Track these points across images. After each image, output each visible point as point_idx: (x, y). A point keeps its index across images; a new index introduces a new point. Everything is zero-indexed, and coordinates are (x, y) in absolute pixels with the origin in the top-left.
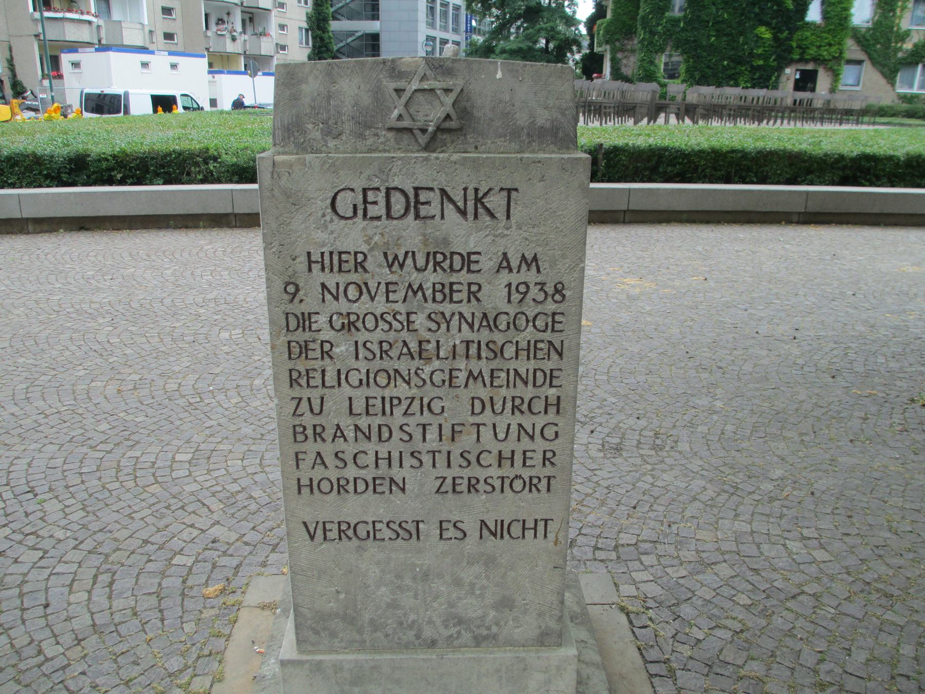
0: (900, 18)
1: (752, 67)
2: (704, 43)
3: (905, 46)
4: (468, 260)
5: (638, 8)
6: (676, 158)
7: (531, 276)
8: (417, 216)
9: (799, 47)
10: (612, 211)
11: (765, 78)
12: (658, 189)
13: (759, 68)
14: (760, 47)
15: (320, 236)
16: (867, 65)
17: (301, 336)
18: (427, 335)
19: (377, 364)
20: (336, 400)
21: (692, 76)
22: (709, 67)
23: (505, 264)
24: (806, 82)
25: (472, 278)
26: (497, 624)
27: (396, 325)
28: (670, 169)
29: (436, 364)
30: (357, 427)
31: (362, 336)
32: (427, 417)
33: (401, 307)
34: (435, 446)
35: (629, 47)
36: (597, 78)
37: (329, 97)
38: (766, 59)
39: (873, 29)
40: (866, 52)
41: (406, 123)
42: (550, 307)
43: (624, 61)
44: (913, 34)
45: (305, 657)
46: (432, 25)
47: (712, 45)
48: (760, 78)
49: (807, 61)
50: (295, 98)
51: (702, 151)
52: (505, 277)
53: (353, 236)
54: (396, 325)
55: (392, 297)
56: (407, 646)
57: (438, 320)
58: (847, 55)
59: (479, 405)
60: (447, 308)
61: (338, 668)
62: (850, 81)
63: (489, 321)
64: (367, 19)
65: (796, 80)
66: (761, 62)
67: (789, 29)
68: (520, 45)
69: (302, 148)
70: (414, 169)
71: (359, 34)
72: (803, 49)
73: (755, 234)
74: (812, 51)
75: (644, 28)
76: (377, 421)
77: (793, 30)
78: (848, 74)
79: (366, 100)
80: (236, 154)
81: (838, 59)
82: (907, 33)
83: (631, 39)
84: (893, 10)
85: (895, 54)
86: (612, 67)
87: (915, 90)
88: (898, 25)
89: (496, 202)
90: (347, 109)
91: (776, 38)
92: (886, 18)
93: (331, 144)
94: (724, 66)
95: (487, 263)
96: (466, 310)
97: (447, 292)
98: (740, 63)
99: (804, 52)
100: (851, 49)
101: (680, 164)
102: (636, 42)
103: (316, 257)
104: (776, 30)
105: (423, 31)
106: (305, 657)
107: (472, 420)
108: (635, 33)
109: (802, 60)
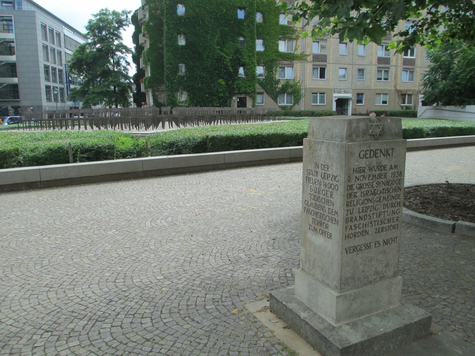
0: (275, 74)
1: (219, 97)
2: (196, 87)
3: (279, 86)
4: (385, 167)
5: (163, 71)
6: (237, 139)
7: (396, 170)
8: (376, 157)
9: (237, 87)
10: (217, 164)
11: (225, 102)
12: (235, 153)
13: (222, 97)
14: (221, 88)
15: (357, 163)
16: (265, 94)
17: (350, 191)
18: (375, 188)
19: (365, 197)
20: (356, 209)
21: (193, 102)
22: (200, 98)
23: (391, 168)
24: (242, 103)
25: (385, 172)
26: (385, 272)
27: (370, 186)
28: (235, 144)
29: (377, 196)
30: (360, 217)
31: (363, 190)
32: (374, 211)
33: (371, 181)
34: (375, 219)
35: (161, 89)
36: (144, 104)
37: (357, 128)
38: (224, 93)
39: (266, 79)
40: (264, 89)
41: (373, 134)
42: (399, 178)
43: (159, 96)
44: (281, 81)
45: (342, 294)
46: (47, 79)
47: (200, 88)
48: (223, 102)
49: (241, 94)
50: (351, 128)
51: (247, 136)
52: (391, 171)
53: (363, 163)
54: (370, 186)
55: (370, 178)
56: (365, 284)
57: (378, 184)
58: (257, 91)
59: (386, 205)
60: (380, 180)
61: (350, 295)
62: (260, 102)
63: (388, 183)
64: (9, 77)
65: (238, 102)
66: (222, 95)
67: (232, 80)
68: (102, 90)
69: (352, 141)
70: (375, 145)
71: (5, 85)
72: (239, 89)
73: (277, 168)
74: (243, 89)
75: (168, 81)
76: (364, 214)
77: (233, 80)
78: (259, 99)
79: (365, 128)
80: (32, 151)
81: (254, 92)
82: (279, 81)
83: (161, 86)
84: (272, 71)
85: (276, 89)
86: (154, 99)
87: (285, 104)
88: (275, 77)
89: (390, 152)
90: (361, 130)
91: (227, 84)
92: (270, 75)
93: (358, 139)
94: (206, 97)
95: (388, 168)
96: (383, 180)
97: (380, 175)
98: (213, 95)
99: (239, 90)
100: (259, 88)
101: (239, 142)
102: (164, 87)
103: (355, 169)
104: (227, 81)
105: (43, 83)
106: (342, 294)
107: (383, 210)
108: (163, 83)
109: (238, 93)
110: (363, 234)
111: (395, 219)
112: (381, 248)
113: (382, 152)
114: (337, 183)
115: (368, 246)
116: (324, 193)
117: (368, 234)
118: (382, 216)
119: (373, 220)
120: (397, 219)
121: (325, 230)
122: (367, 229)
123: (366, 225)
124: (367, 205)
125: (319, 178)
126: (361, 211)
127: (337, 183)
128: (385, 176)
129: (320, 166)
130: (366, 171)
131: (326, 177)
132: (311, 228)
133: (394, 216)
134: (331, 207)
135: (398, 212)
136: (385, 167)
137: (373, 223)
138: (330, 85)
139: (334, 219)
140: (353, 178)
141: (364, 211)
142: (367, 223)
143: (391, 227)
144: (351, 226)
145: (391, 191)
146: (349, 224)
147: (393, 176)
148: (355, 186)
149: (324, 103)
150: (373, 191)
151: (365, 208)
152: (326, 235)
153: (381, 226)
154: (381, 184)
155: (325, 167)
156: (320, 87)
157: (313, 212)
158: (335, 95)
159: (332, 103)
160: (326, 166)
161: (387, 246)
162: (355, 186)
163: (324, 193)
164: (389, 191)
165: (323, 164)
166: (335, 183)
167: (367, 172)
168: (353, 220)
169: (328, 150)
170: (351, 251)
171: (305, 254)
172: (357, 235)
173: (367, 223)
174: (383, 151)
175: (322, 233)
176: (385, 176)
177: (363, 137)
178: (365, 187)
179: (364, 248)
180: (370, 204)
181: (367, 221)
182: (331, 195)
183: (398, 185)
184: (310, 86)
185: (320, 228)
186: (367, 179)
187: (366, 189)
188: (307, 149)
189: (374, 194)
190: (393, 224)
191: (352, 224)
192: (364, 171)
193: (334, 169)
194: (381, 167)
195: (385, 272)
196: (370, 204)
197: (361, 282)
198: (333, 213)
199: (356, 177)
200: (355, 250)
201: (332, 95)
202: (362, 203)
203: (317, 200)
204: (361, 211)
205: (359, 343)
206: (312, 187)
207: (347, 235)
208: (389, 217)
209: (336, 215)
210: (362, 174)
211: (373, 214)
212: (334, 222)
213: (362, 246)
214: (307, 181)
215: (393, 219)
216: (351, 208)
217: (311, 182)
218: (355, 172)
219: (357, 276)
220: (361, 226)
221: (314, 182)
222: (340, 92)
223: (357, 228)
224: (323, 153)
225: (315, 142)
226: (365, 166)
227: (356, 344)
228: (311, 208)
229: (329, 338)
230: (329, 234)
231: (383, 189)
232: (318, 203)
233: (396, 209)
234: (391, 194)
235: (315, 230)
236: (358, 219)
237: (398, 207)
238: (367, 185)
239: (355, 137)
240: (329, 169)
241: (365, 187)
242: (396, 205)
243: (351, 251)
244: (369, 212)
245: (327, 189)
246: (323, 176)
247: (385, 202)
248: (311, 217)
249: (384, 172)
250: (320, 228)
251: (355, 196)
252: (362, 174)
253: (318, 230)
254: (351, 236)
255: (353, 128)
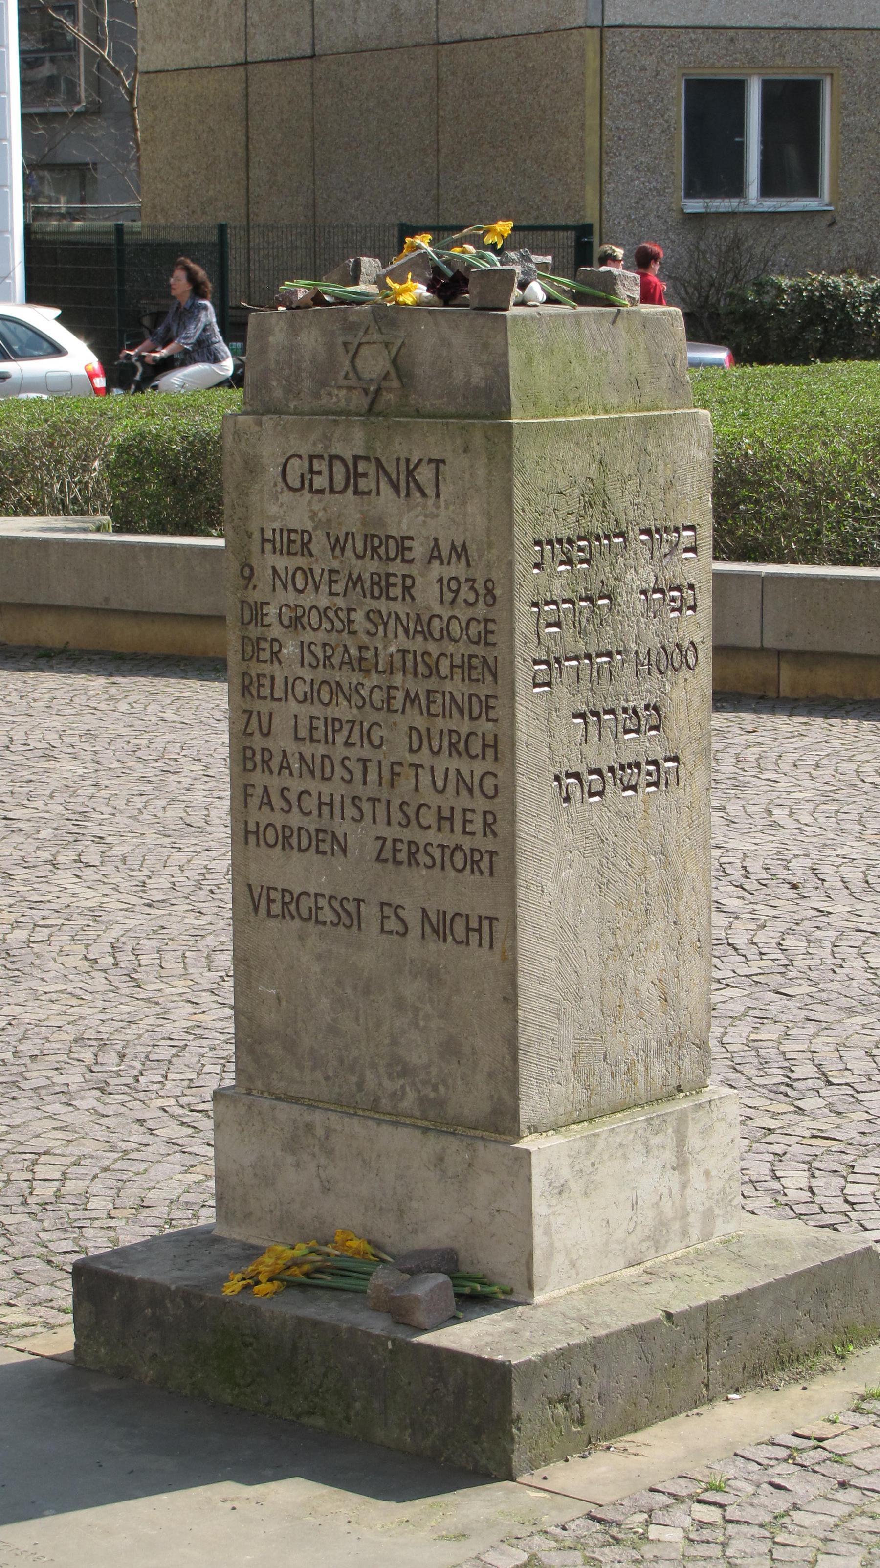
4: (402, 545)
7: (457, 569)
18: (365, 639)
23: (435, 555)
31: (308, 636)
33: (340, 602)
54: (338, 625)
55: (336, 588)
76: (321, 749)
89: (425, 475)
90: (306, 364)
95: (418, 550)
96: (400, 608)
103: (269, 535)
110: (323, 847)
118: (406, 784)
119: (358, 788)
122: (341, 827)
130: (314, 547)
135: (489, 789)
136: (402, 545)
137: (366, 807)
143: (459, 858)
147: (448, 596)
149: (813, 190)
150: (353, 651)
173: (337, 799)
174: (391, 469)
177: (317, 396)
186: (324, 588)
191: (275, 783)
192: (305, 545)
196: (342, 710)
204: (303, 733)
216: (264, 707)
218: (268, 547)
234: (448, 687)
237: (488, 765)
238: (323, 613)
249: (398, 568)
255: (272, 355)
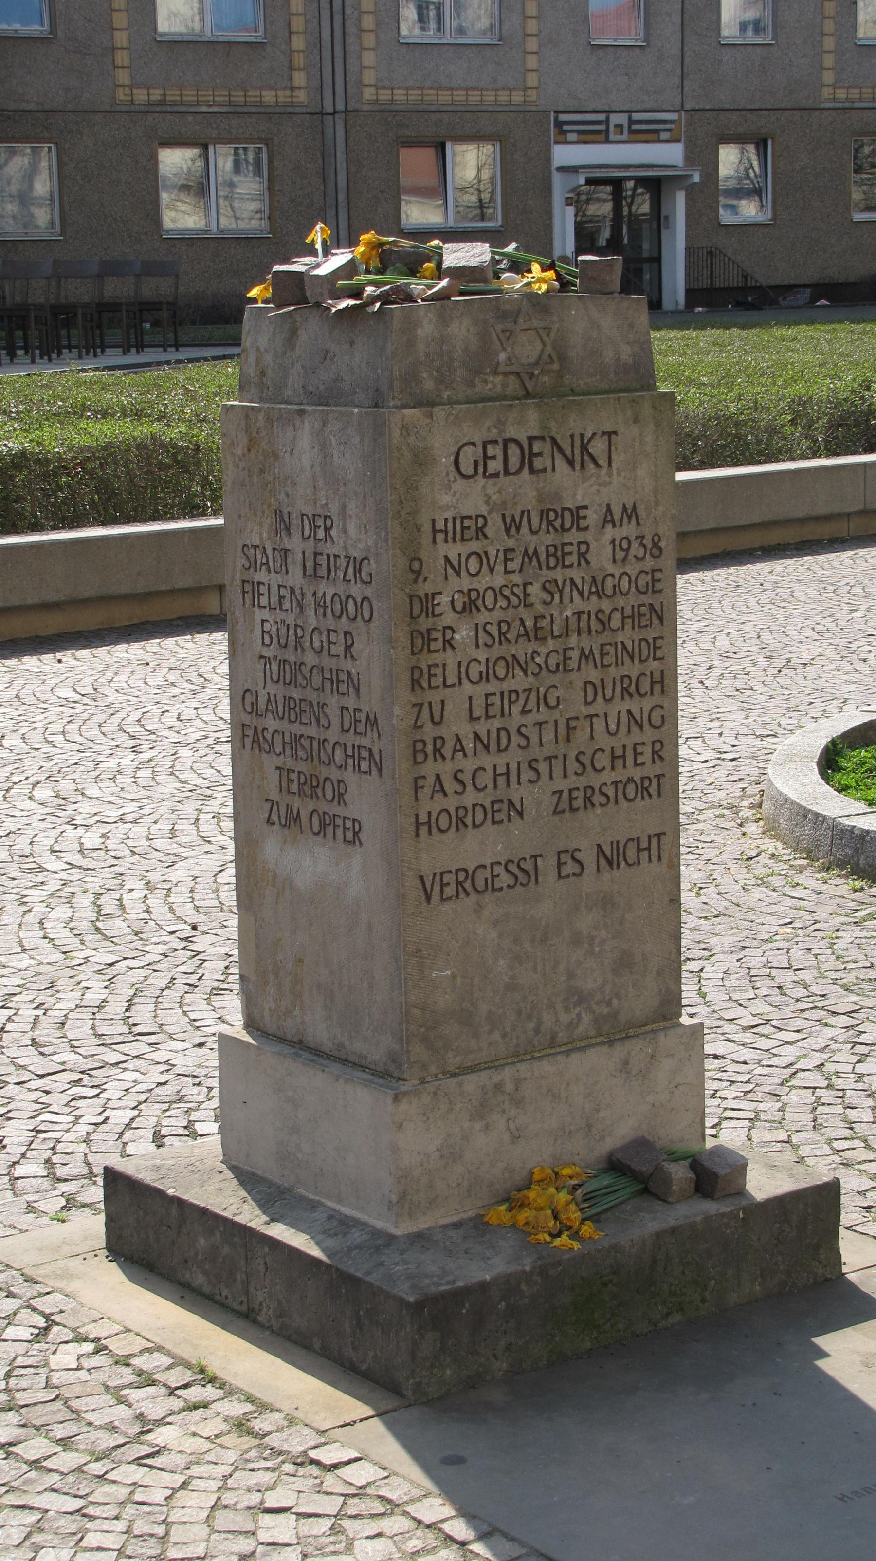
4: (577, 515)
7: (629, 530)
8: (532, 471)
18: (540, 608)
19: (498, 651)
23: (608, 519)
26: (618, 996)
27: (514, 600)
30: (477, 736)
31: (482, 617)
32: (544, 714)
33: (516, 578)
41: (514, 368)
52: (610, 532)
54: (514, 600)
55: (511, 566)
60: (558, 575)
70: (525, 424)
76: (497, 723)
89: (598, 447)
95: (592, 517)
96: (576, 574)
97: (558, 555)
103: (440, 525)
107: (585, 711)
111: (648, 750)
112: (588, 883)
113: (560, 450)
114: (369, 592)
115: (524, 872)
116: (317, 644)
117: (521, 814)
118: (581, 736)
119: (535, 751)
120: (654, 752)
121: (335, 809)
123: (507, 774)
124: (506, 686)
125: (295, 578)
126: (478, 712)
127: (369, 592)
128: (582, 555)
129: (296, 522)
130: (488, 531)
131: (323, 572)
132: (275, 818)
133: (636, 736)
134: (351, 702)
136: (577, 515)
137: (543, 767)
138: (532, 80)
139: (365, 754)
140: (434, 567)
141: (495, 710)
142: (514, 767)
144: (438, 777)
145: (616, 622)
146: (430, 768)
147: (620, 555)
148: (444, 599)
150: (529, 623)
151: (497, 700)
152: (340, 832)
153: (582, 782)
154: (567, 589)
155: (320, 523)
156: (460, 96)
157: (278, 740)
158: (565, 154)
159: (548, 213)
160: (320, 522)
161: (616, 873)
162: (444, 599)
163: (317, 644)
164: (604, 624)
165: (309, 510)
166: (356, 590)
167: (498, 539)
168: (447, 751)
169: (324, 447)
170: (450, 891)
171: (258, 946)
172: (469, 820)
173: (514, 767)
175: (323, 826)
176: (582, 555)
178: (489, 602)
179: (504, 880)
180: (519, 681)
181: (514, 757)
182: (348, 648)
183: (647, 599)
184: (385, 95)
185: (311, 805)
187: (498, 614)
188: (239, 451)
189: (537, 634)
190: (638, 774)
191: (446, 769)
193: (352, 529)
194: (560, 517)
195: (618, 996)
196: (519, 681)
197: (504, 1036)
198: (361, 728)
199: (447, 559)
200: (468, 885)
201: (548, 159)
202: (484, 678)
203: (293, 682)
204: (478, 712)
205: (494, 1280)
206: (267, 627)
207: (423, 818)
208: (616, 743)
209: (372, 734)
210: (474, 546)
211: (540, 724)
212: (364, 766)
213: (498, 870)
214: (248, 597)
215: (636, 754)
216: (434, 697)
217: (264, 601)
218: (440, 537)
219: (484, 1008)
220: (485, 779)
221: (274, 600)
222: (601, 136)
223: (470, 788)
224: (306, 461)
225: (269, 420)
226: (484, 510)
227: (483, 1286)
228: (272, 724)
229: (369, 1273)
230: (349, 824)
231: (579, 614)
232: (296, 694)
233: (647, 703)
234: (620, 637)
235: (292, 820)
236: (469, 746)
237: (656, 700)
238: (498, 593)
239: (429, 385)
240: (333, 532)
241: (489, 602)
242: (645, 686)
243: (450, 891)
244: (517, 719)
245: (331, 623)
246: (310, 564)
247: (594, 675)
248: (270, 762)
249: (573, 536)
250: (311, 805)
251: (449, 644)
252: (474, 546)
253: (304, 818)
254: (444, 824)
255: (421, 347)
